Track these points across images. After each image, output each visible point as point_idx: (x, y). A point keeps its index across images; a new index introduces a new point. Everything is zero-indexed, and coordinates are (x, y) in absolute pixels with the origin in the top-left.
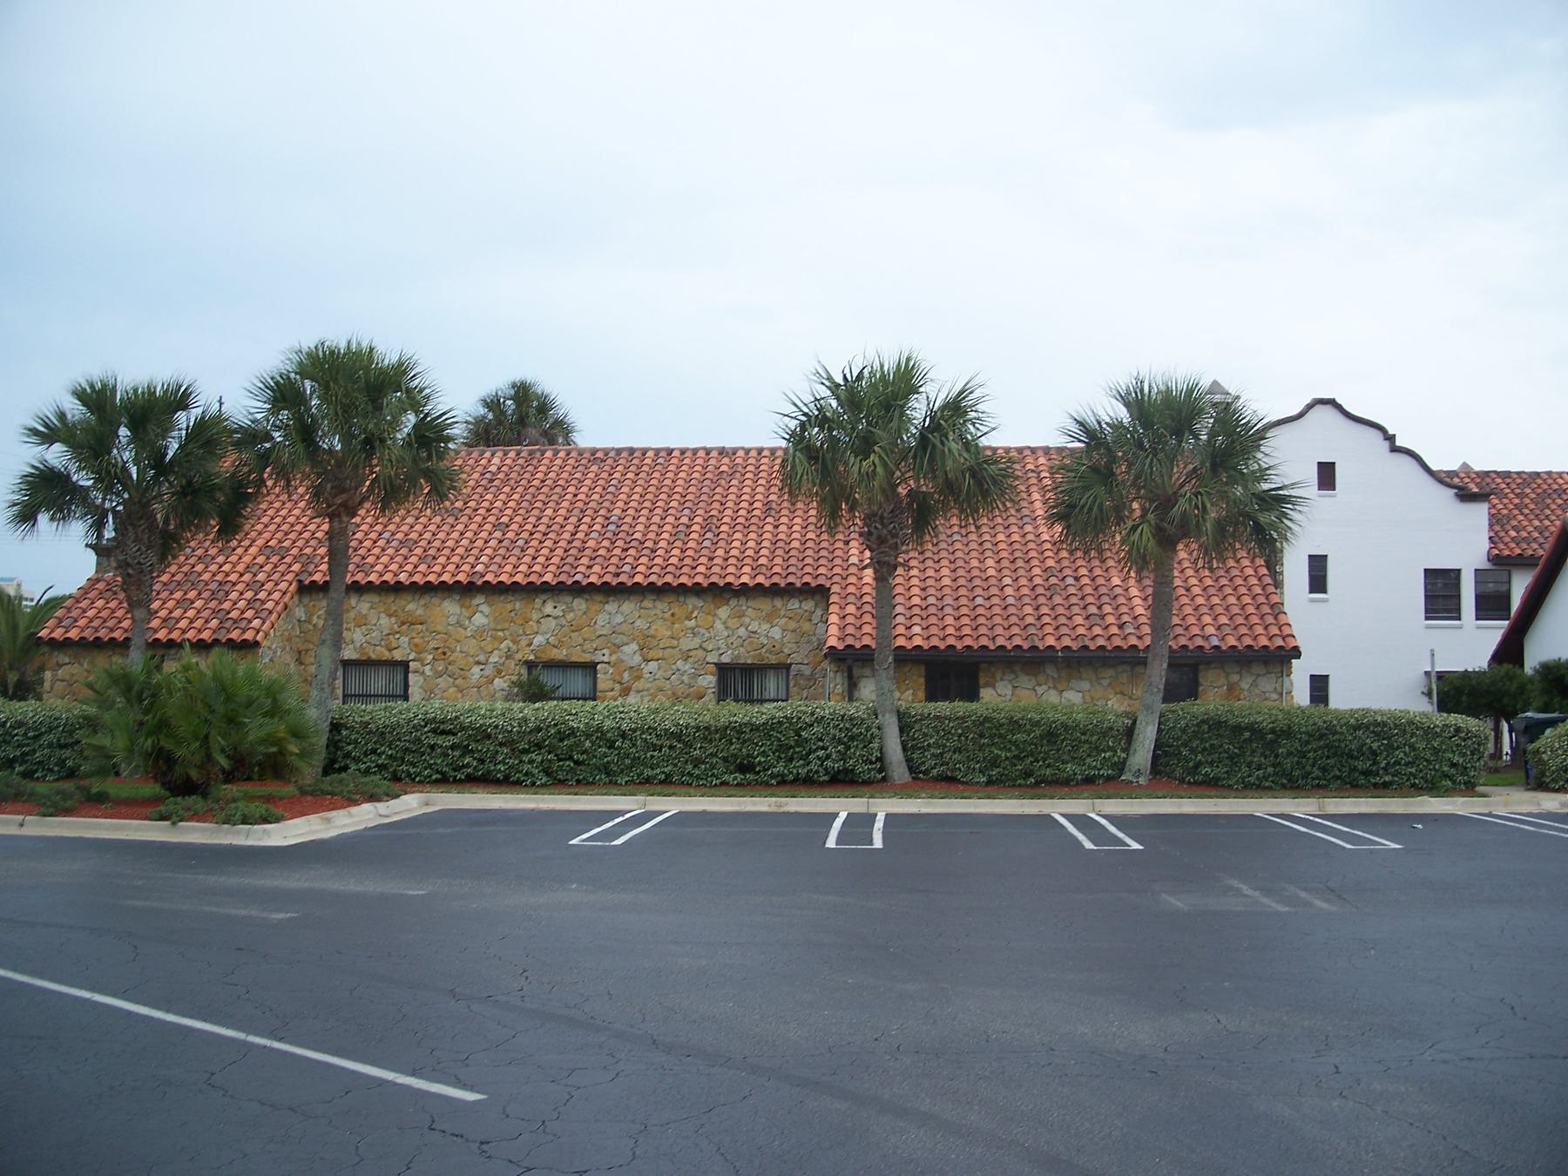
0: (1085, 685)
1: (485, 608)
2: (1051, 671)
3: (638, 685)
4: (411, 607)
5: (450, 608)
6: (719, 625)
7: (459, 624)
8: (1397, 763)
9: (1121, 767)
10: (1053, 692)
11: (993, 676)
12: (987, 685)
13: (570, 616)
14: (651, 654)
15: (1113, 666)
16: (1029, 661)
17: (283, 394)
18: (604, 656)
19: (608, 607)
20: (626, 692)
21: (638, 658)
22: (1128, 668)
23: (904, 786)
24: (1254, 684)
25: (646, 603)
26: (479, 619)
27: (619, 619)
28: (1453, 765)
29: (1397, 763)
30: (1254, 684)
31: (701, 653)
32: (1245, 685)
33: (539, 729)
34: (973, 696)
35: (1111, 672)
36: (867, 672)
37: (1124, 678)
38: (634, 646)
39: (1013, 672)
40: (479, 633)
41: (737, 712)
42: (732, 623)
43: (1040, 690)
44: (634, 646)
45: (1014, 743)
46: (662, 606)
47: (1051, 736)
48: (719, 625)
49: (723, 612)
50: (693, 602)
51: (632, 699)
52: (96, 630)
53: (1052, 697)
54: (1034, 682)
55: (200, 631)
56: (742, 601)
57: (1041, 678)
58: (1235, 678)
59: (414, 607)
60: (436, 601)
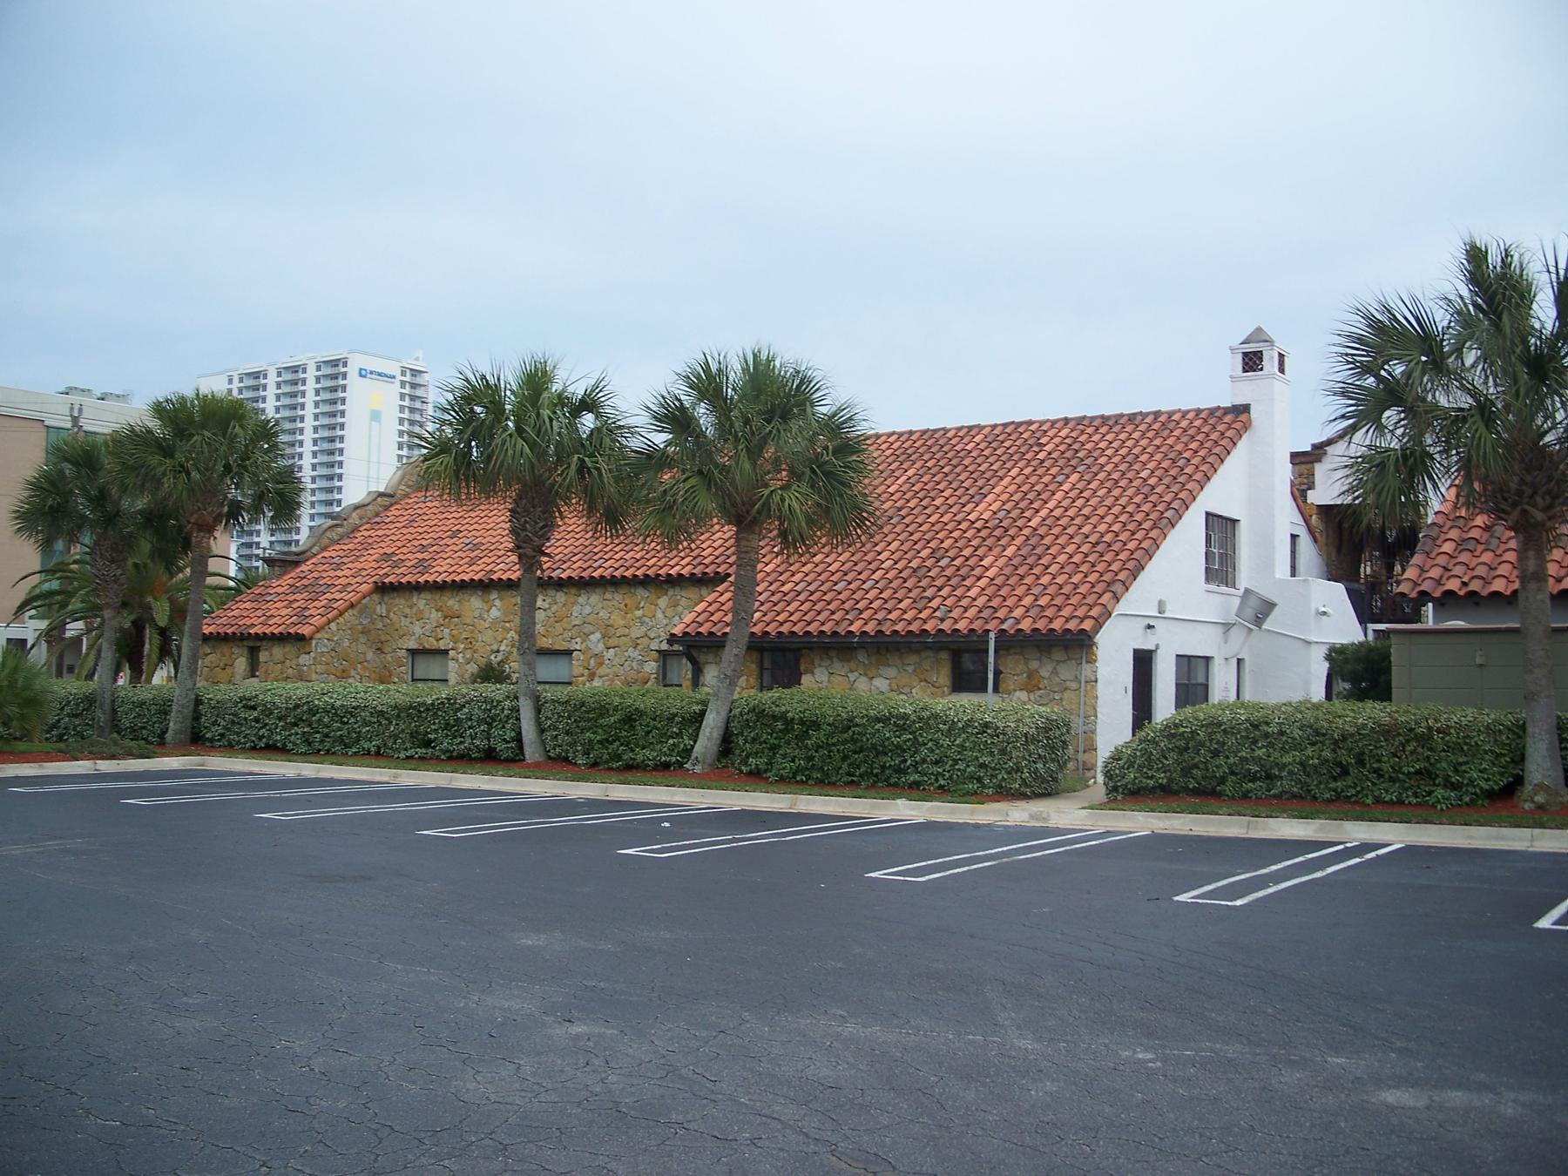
0: (892, 672)
1: (497, 603)
2: (862, 656)
3: (601, 671)
4: (450, 603)
5: (475, 602)
6: (659, 615)
7: (481, 617)
8: (924, 761)
9: (688, 752)
10: (863, 679)
11: (812, 662)
12: (807, 672)
13: (554, 608)
14: (612, 642)
15: (917, 652)
16: (840, 647)
17: (675, 418)
18: (576, 645)
19: (581, 600)
20: (592, 677)
21: (601, 646)
22: (930, 653)
23: (537, 765)
24: (1055, 672)
25: (608, 596)
26: (494, 613)
27: (588, 610)
28: (983, 766)
29: (924, 761)
30: (1055, 672)
31: (646, 640)
32: (1044, 673)
33: (297, 706)
34: (793, 680)
35: (914, 658)
36: (710, 658)
37: (926, 665)
38: (598, 635)
39: (831, 658)
40: (495, 622)
41: (1372, 712)
42: (669, 612)
43: (852, 677)
44: (598, 635)
45: (601, 726)
46: (616, 598)
47: (629, 720)
48: (659, 615)
49: (663, 602)
50: (641, 593)
51: (596, 683)
52: (1018, 621)
53: (862, 685)
54: (846, 669)
55: (956, 621)
56: (677, 590)
57: (853, 664)
58: (1034, 665)
59: (452, 602)
60: (466, 597)
